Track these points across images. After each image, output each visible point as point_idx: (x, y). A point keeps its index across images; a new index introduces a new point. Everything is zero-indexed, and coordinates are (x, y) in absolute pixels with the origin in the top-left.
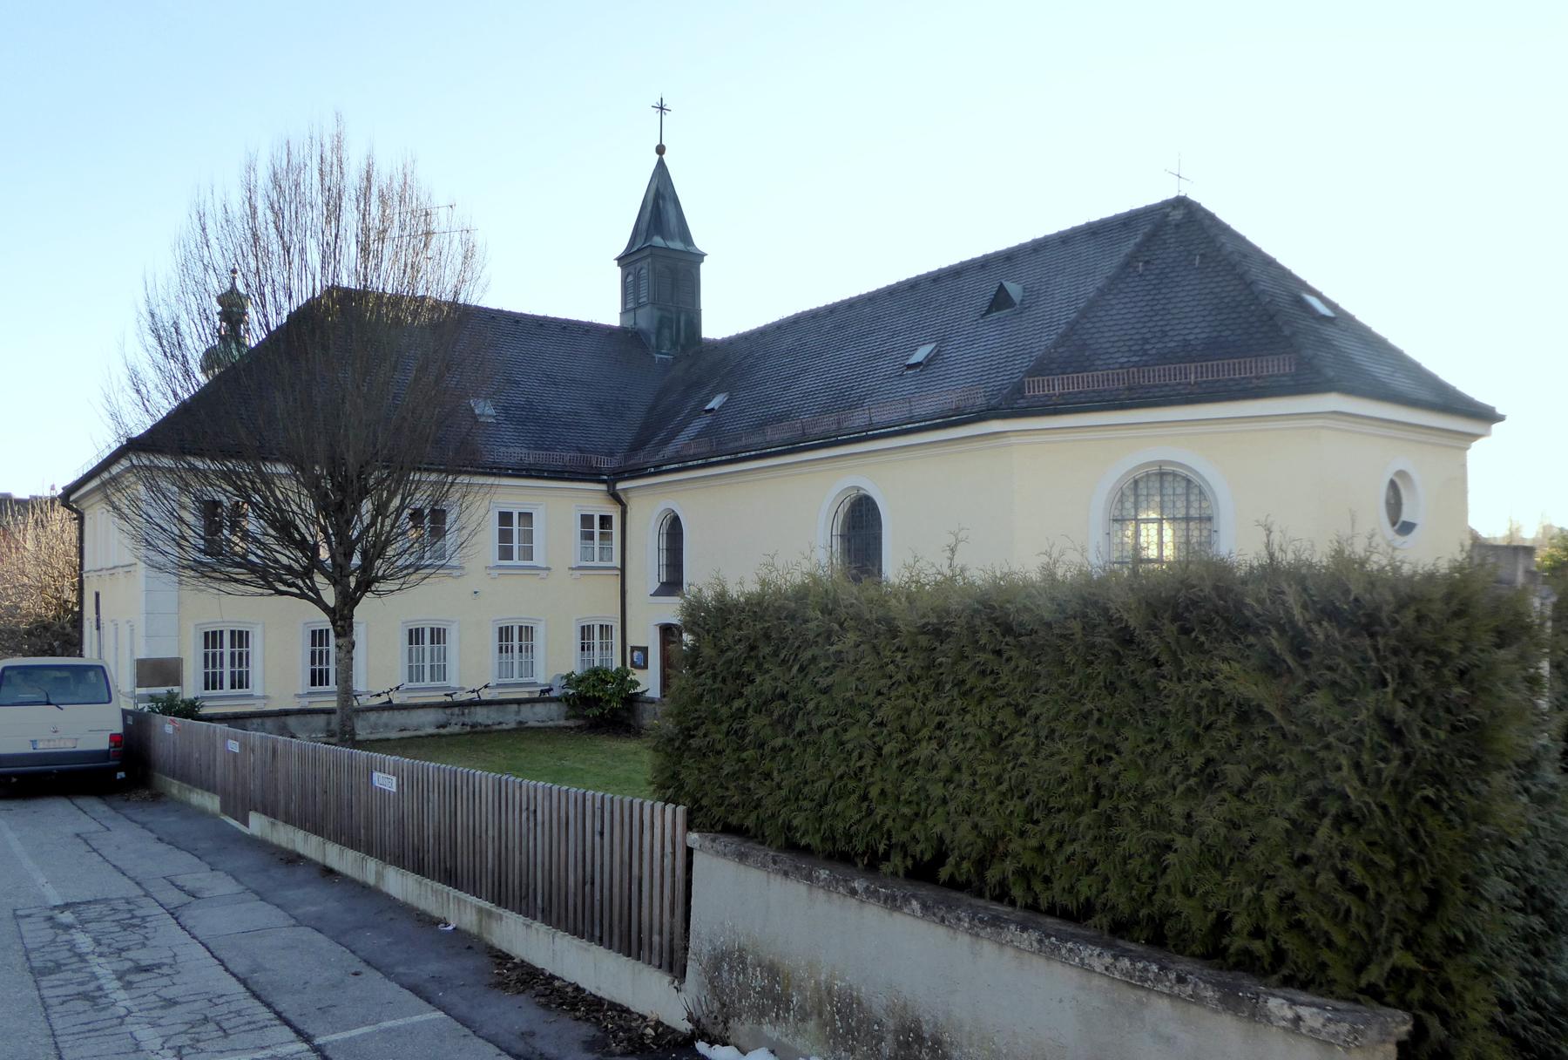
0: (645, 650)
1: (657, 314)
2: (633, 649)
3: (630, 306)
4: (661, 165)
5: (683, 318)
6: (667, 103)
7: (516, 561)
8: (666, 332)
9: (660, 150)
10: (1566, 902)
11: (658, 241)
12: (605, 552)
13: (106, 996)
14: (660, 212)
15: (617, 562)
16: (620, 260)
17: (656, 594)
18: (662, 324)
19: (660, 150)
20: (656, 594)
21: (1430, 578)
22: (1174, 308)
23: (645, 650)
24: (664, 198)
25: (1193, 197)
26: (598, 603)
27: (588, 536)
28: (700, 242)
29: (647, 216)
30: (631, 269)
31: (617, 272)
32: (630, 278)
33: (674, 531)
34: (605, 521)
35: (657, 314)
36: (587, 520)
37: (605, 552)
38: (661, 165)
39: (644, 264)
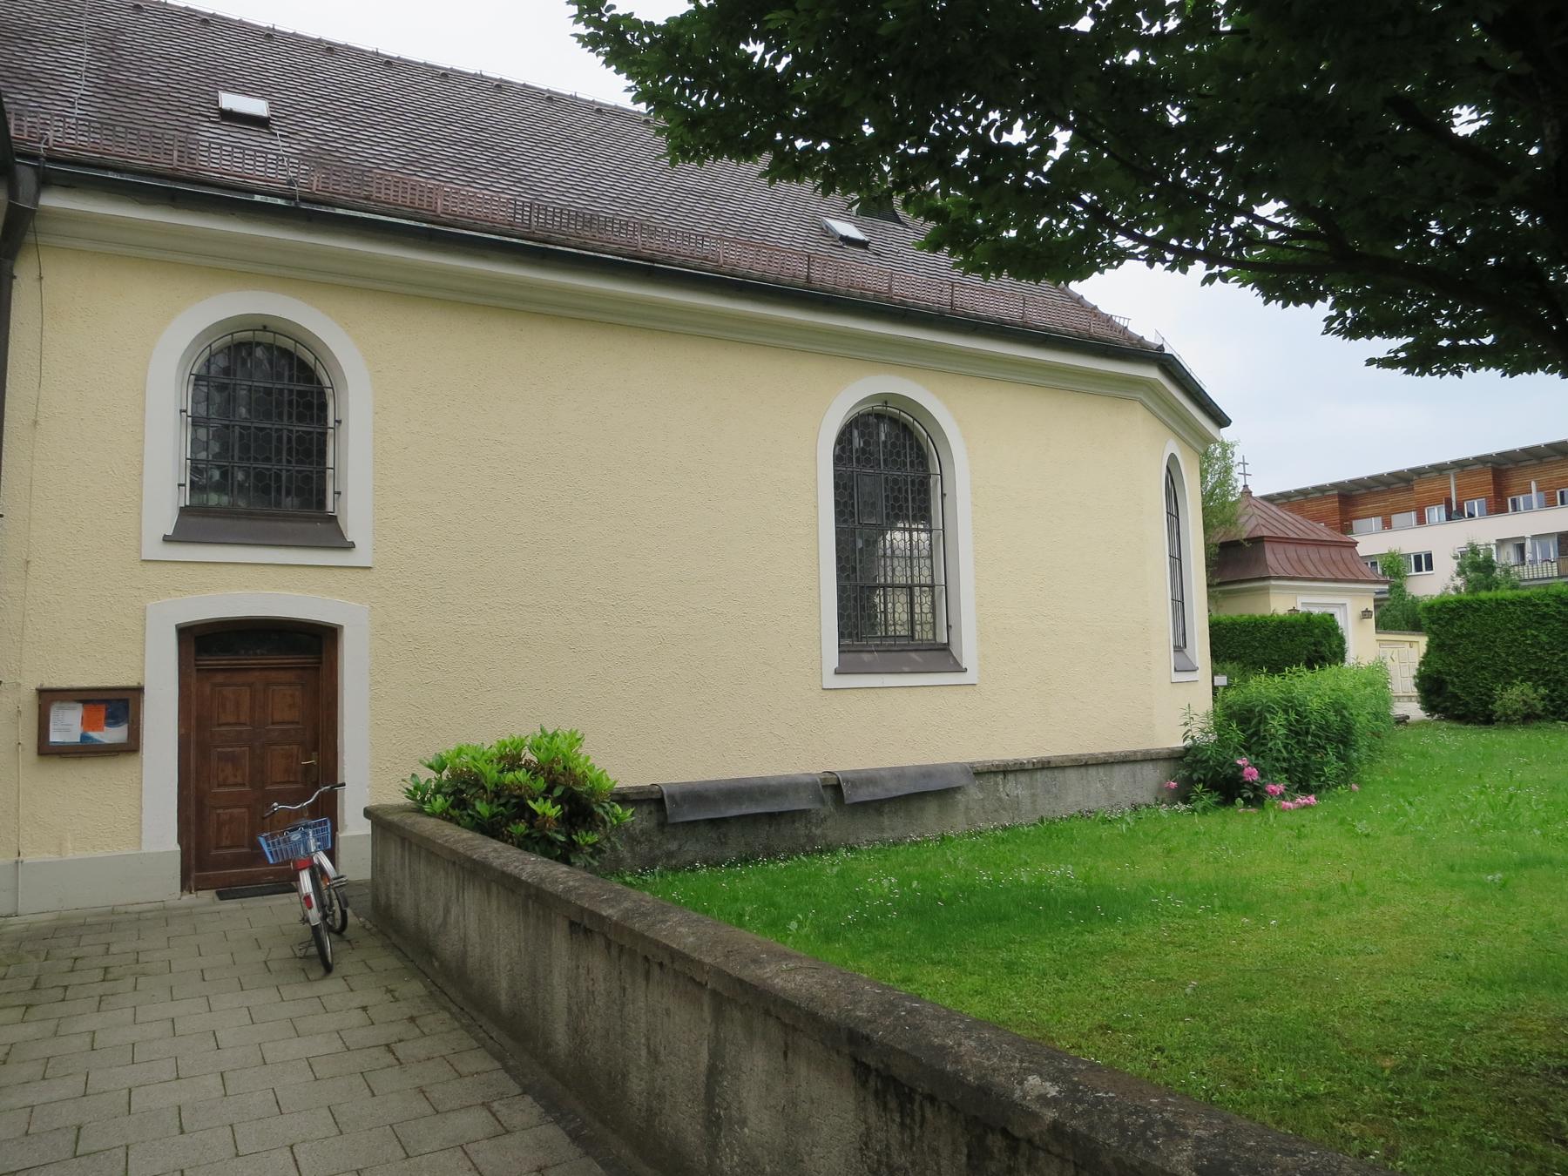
14: (1203, 283)
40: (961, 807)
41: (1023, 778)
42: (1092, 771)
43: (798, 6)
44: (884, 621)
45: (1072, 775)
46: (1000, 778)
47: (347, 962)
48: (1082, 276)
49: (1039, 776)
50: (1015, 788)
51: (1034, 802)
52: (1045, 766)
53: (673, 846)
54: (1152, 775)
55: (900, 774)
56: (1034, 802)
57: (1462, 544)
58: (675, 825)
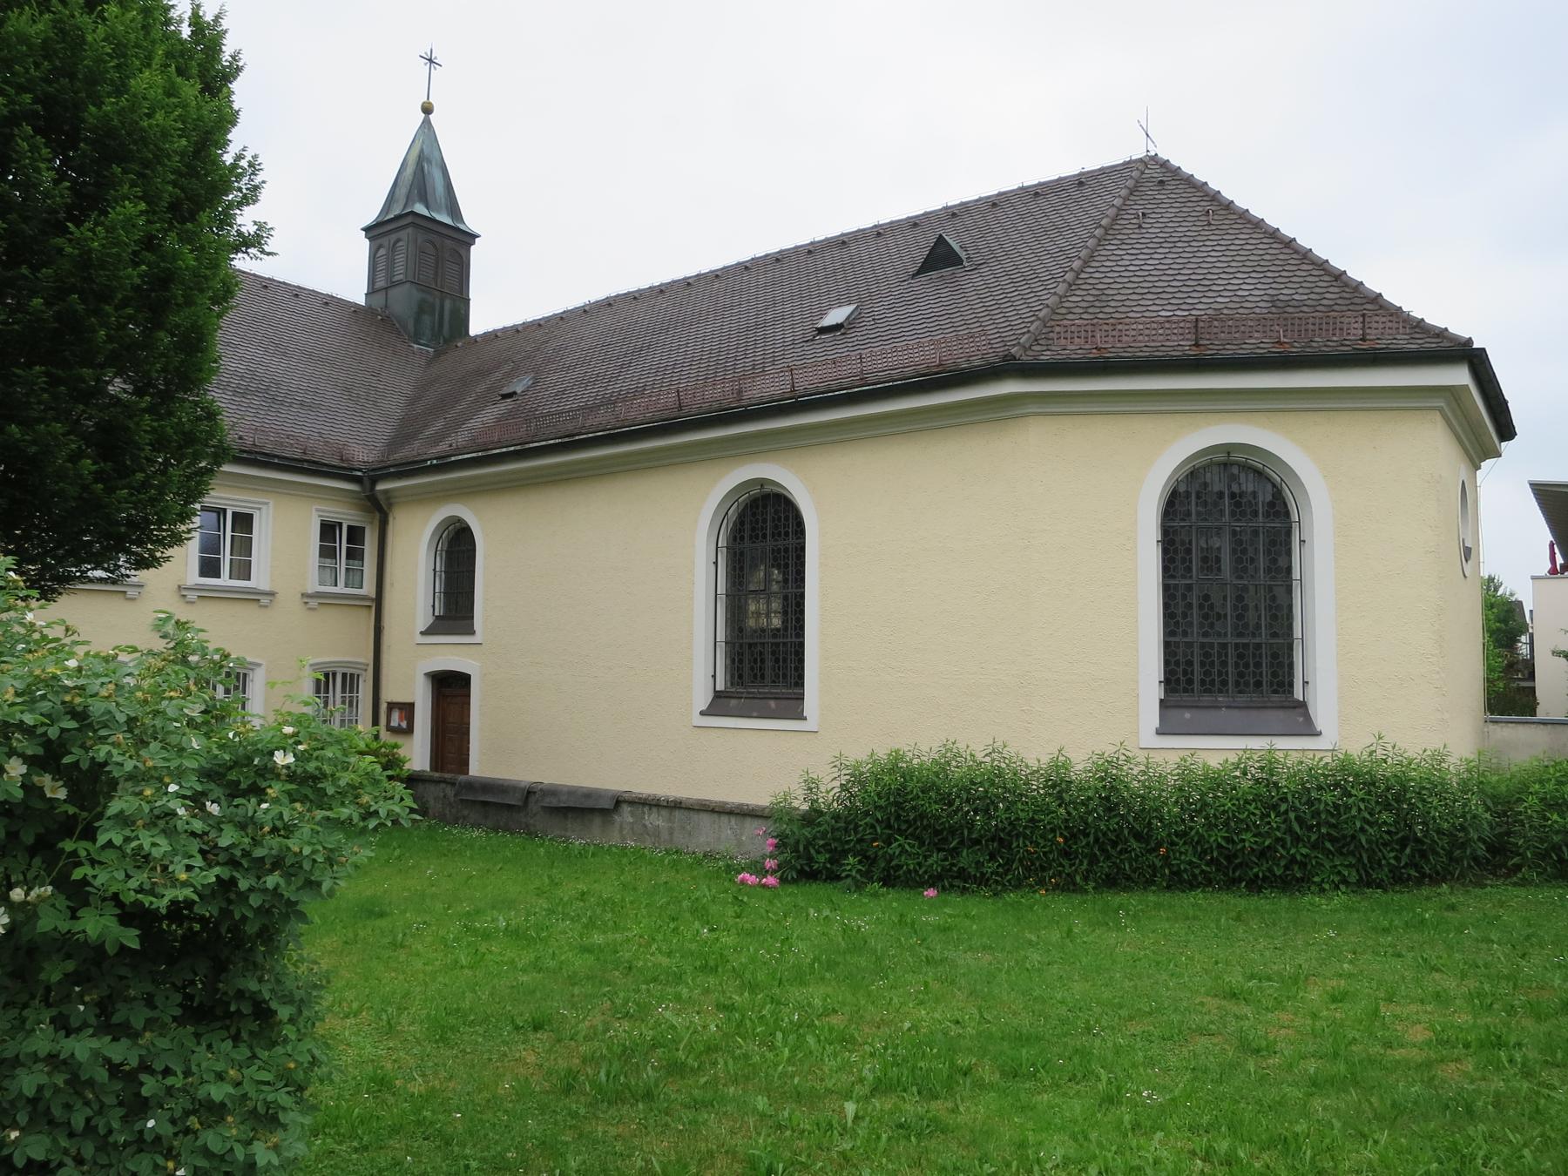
0: (408, 709)
1: (417, 295)
2: (392, 706)
3: (380, 284)
4: (426, 124)
5: (448, 304)
6: (439, 56)
7: (224, 580)
8: (426, 319)
9: (427, 109)
10: (866, 1174)
11: (420, 209)
12: (354, 577)
13: (90, 834)
14: (423, 176)
15: (369, 588)
16: (367, 230)
17: (428, 632)
18: (422, 309)
19: (427, 109)
20: (428, 632)
21: (1058, 784)
22: (1124, 297)
23: (408, 709)
24: (429, 162)
25: (1163, 155)
26: (342, 641)
27: (327, 552)
28: (471, 220)
29: (410, 171)
30: (385, 241)
31: (365, 245)
32: (382, 252)
33: (457, 549)
34: (355, 535)
35: (417, 295)
36: (328, 530)
37: (354, 577)
38: (426, 124)
39: (403, 234)
40: (617, 825)
41: (664, 812)
42: (724, 819)
43: (1563, 1020)
44: (763, 666)
45: (705, 818)
46: (646, 809)
47: (79, 914)
48: (195, 182)
49: (677, 813)
50: (655, 820)
51: (671, 834)
52: (676, 806)
53: (466, 812)
54: (757, 841)
55: (572, 792)
56: (671, 834)
57: (151, 617)
58: (1466, 496)
